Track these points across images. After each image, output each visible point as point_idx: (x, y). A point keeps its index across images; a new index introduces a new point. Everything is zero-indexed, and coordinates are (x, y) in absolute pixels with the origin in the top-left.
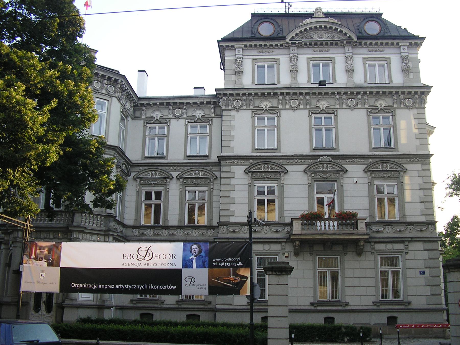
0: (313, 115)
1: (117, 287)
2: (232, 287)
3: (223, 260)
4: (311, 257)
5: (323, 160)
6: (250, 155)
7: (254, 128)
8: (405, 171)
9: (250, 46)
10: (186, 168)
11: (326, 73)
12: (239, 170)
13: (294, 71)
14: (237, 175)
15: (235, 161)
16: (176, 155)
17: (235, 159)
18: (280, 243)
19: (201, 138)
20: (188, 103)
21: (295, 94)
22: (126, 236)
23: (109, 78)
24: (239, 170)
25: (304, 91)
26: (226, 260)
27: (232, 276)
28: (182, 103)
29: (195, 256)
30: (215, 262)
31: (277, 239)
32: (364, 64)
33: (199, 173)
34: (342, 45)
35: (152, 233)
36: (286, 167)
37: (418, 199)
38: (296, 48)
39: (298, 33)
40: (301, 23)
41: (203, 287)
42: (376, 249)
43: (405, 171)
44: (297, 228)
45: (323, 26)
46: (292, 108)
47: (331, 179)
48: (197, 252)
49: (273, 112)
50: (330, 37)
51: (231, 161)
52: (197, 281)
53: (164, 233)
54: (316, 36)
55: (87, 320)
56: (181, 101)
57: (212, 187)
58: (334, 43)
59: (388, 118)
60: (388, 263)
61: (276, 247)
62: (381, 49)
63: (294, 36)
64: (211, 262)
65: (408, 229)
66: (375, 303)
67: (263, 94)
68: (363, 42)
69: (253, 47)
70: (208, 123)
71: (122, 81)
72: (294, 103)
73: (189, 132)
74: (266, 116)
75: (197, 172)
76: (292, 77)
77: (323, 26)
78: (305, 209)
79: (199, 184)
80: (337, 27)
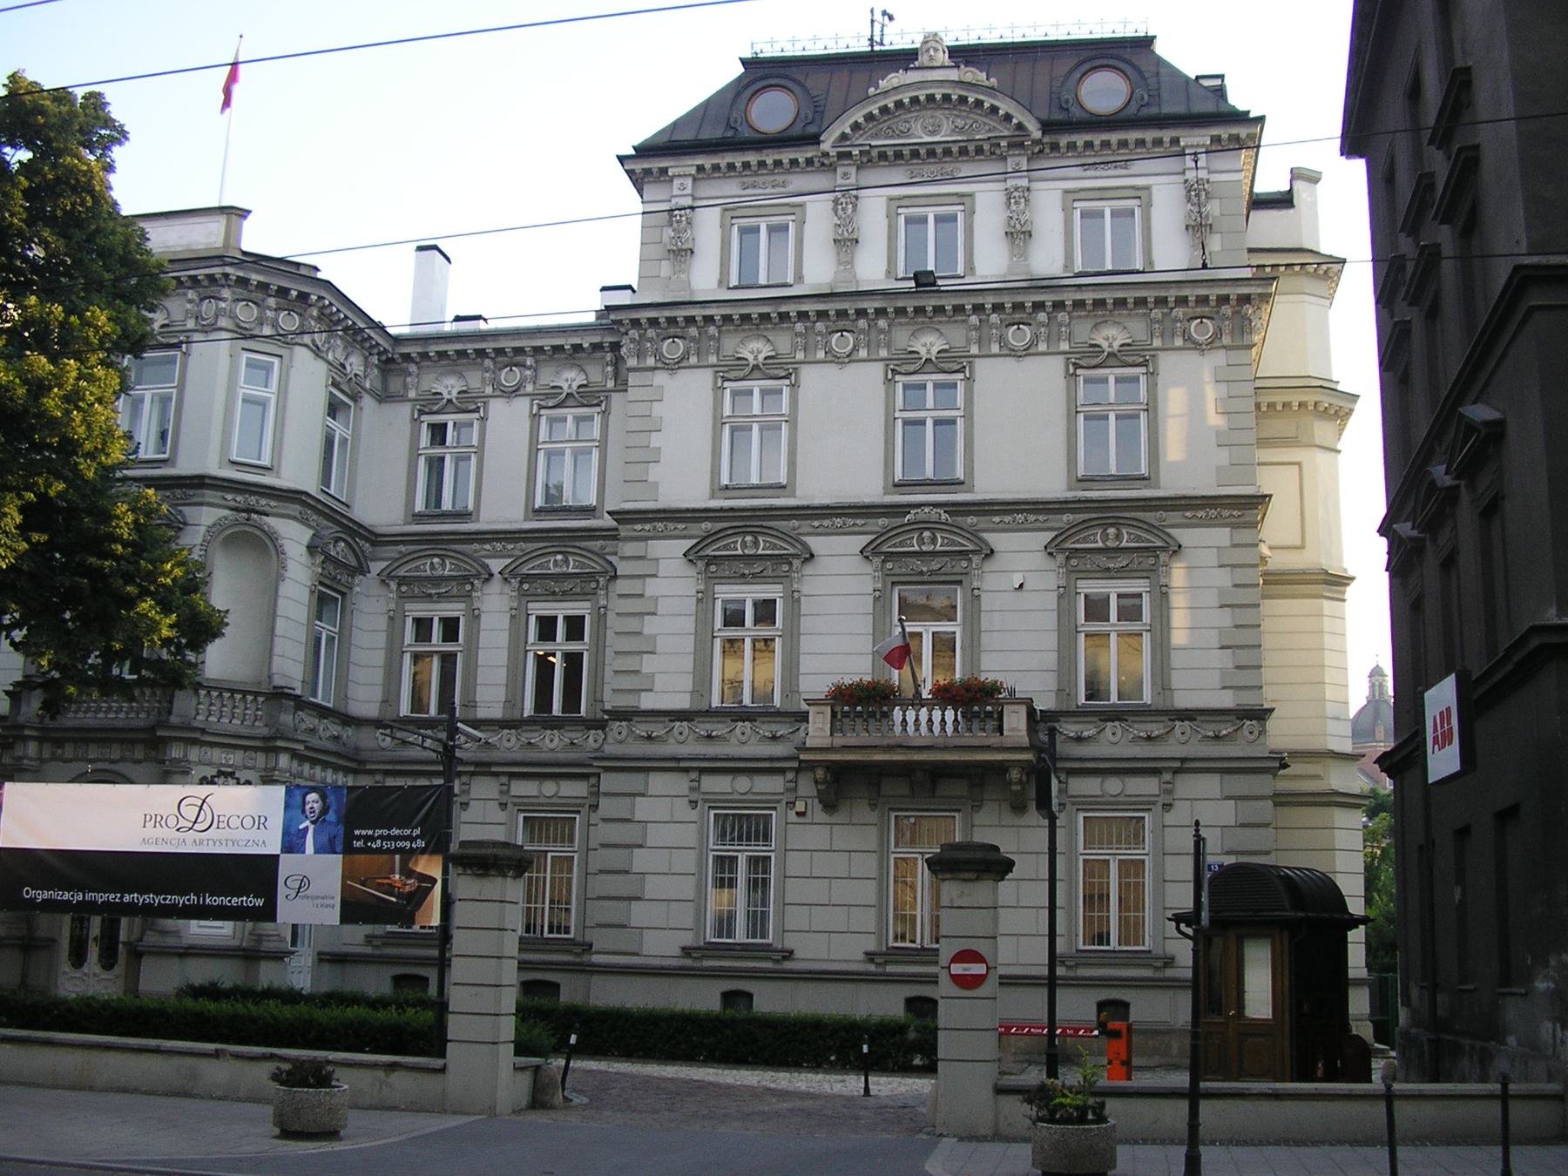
0: (898, 378)
1: (127, 898)
3: (378, 832)
4: (873, 817)
5: (919, 518)
9: (716, 168)
11: (945, 249)
12: (670, 551)
13: (846, 243)
14: (665, 568)
16: (503, 507)
18: (782, 771)
20: (538, 350)
21: (842, 314)
22: (357, 749)
23: (283, 292)
24: (670, 551)
25: (870, 305)
26: (385, 832)
28: (519, 351)
30: (359, 838)
31: (771, 759)
32: (1067, 211)
33: (566, 562)
37: (1213, 639)
38: (853, 170)
39: (861, 120)
42: (1071, 792)
44: (818, 730)
45: (938, 97)
46: (834, 359)
47: (943, 578)
50: (961, 130)
51: (647, 527)
52: (314, 889)
54: (917, 128)
55: (211, 991)
56: (517, 344)
57: (603, 602)
58: (971, 148)
60: (1119, 836)
63: (848, 131)
64: (349, 837)
65: (1178, 731)
67: (746, 318)
68: (1064, 140)
69: (1114, 147)
71: (321, 298)
72: (1018, 337)
74: (756, 386)
75: (559, 557)
76: (840, 263)
77: (938, 97)
78: (859, 668)
80: (981, 97)
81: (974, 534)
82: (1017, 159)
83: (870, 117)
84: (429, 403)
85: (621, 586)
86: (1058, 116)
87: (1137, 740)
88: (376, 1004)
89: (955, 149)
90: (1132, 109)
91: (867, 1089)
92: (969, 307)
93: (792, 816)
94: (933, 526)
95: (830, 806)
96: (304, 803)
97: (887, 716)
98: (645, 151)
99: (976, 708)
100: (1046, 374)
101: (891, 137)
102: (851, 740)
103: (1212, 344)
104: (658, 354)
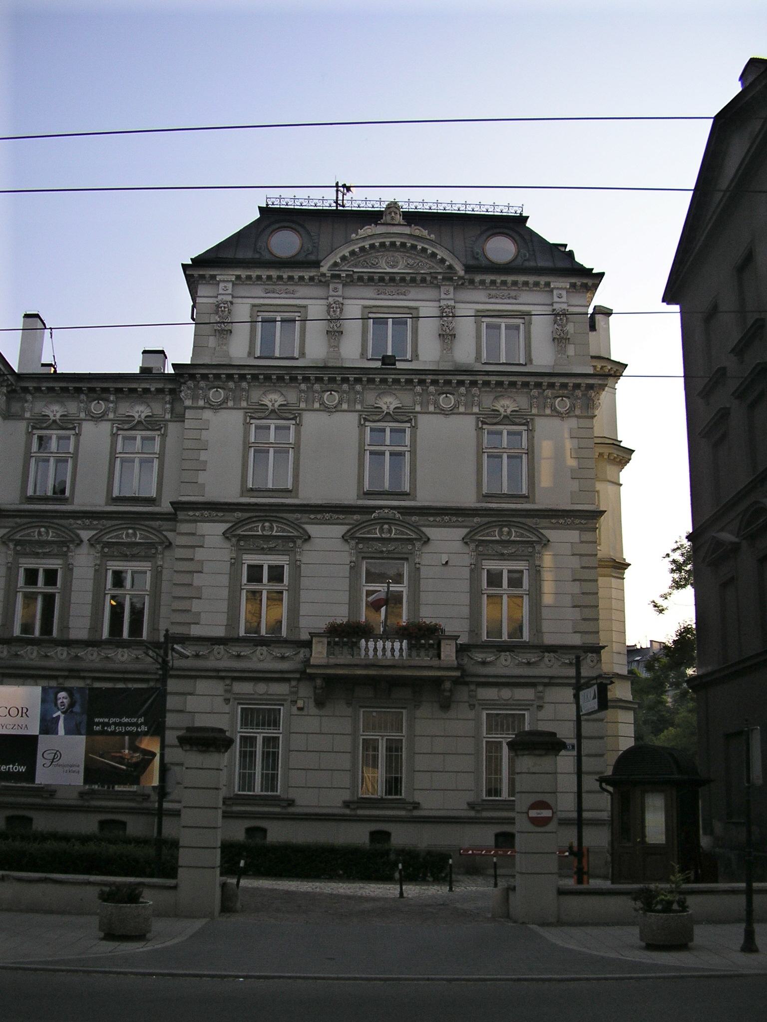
2: (127, 770)
3: (112, 720)
6: (235, 501)
7: (247, 446)
8: (545, 543)
9: (249, 278)
10: (109, 523)
11: (399, 340)
12: (212, 531)
14: (208, 541)
15: (206, 513)
16: (89, 495)
17: (205, 509)
18: (288, 680)
19: (142, 461)
24: (212, 531)
27: (127, 751)
29: (63, 713)
30: (98, 724)
31: (281, 672)
33: (135, 535)
34: (435, 282)
35: (35, 653)
36: (308, 528)
38: (340, 286)
40: (354, 235)
41: (74, 769)
42: (479, 697)
43: (545, 543)
44: (319, 653)
45: (398, 244)
46: (325, 409)
47: (396, 556)
48: (66, 705)
49: (287, 415)
53: (59, 654)
54: (383, 263)
57: (160, 563)
58: (419, 278)
59: (520, 434)
61: (280, 689)
62: (513, 294)
63: (339, 260)
65: (546, 659)
66: (471, 806)
68: (478, 278)
69: (254, 279)
70: (159, 433)
72: (331, 398)
73: (119, 448)
74: (273, 423)
75: (130, 531)
76: (331, 347)
78: (341, 615)
79: (133, 556)
81: (416, 528)
82: (447, 288)
83: (353, 253)
84: (40, 422)
85: (179, 553)
86: (472, 262)
87: (520, 664)
88: (85, 839)
89: (408, 278)
90: (519, 261)
91: (401, 893)
92: (300, 377)
93: (294, 710)
94: (390, 521)
95: (320, 703)
96: (56, 699)
97: (356, 645)
98: (200, 262)
99: (423, 641)
100: (463, 427)
101: (366, 267)
102: (341, 660)
103: (569, 414)
104: (206, 398)
